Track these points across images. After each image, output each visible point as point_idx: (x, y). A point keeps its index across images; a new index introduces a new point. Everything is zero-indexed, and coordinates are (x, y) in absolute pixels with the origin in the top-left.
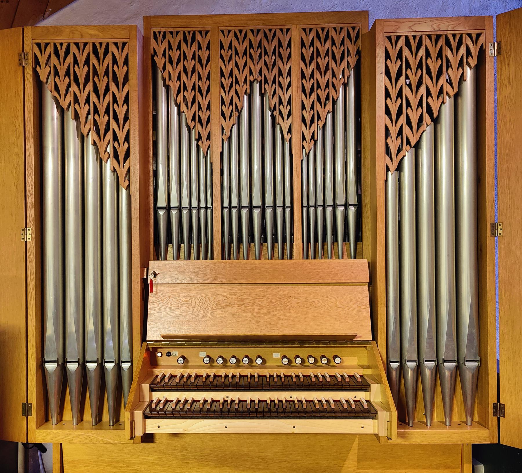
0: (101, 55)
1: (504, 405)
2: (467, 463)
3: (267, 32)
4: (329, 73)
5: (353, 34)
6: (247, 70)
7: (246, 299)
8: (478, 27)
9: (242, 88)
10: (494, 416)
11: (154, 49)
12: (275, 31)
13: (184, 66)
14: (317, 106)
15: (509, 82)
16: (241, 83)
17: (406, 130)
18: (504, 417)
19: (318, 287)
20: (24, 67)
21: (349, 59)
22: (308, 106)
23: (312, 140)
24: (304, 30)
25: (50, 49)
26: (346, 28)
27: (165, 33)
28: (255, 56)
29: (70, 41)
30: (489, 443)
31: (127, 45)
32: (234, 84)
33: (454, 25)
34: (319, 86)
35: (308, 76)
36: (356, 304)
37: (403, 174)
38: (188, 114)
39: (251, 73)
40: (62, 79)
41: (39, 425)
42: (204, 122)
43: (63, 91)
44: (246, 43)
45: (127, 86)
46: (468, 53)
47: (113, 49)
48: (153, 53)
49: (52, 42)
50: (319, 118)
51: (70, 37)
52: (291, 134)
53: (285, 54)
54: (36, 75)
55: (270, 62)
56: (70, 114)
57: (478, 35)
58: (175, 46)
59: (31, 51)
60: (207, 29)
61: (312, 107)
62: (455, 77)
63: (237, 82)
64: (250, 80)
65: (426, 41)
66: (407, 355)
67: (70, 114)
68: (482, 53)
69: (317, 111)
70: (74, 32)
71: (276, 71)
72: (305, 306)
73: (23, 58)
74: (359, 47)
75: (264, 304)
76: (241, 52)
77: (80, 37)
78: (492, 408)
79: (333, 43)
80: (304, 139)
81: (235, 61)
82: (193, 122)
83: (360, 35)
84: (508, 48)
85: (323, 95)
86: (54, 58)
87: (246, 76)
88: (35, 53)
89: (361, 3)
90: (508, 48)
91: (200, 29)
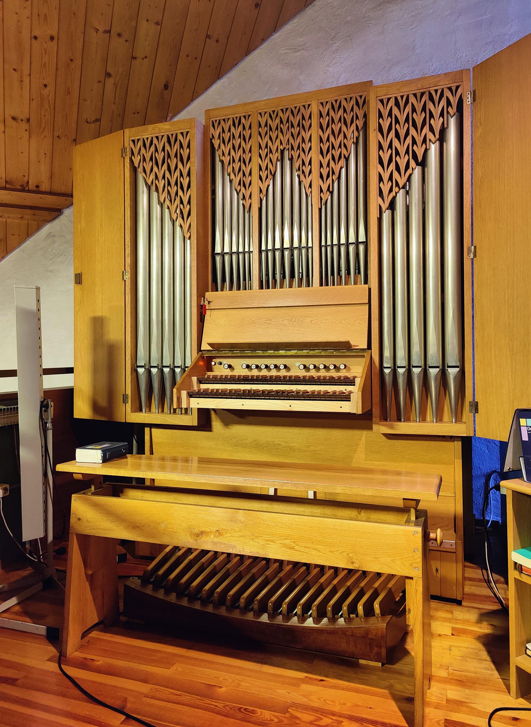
0: (173, 143)
1: (478, 402)
2: (457, 459)
3: (293, 109)
4: (342, 135)
5: (361, 102)
6: (278, 141)
7: (273, 319)
8: (456, 80)
9: (275, 156)
10: (470, 412)
11: (212, 134)
12: (299, 107)
13: (233, 144)
14: (332, 163)
15: (481, 124)
16: (274, 152)
17: (396, 175)
18: (478, 413)
19: (328, 308)
20: (124, 158)
21: (357, 122)
22: (325, 164)
23: (328, 192)
24: (322, 104)
25: (140, 143)
26: (355, 97)
27: (220, 120)
28: (285, 129)
29: (152, 135)
30: (466, 435)
31: (189, 133)
32: (269, 153)
33: (435, 82)
34: (333, 147)
35: (325, 140)
36: (357, 321)
37: (395, 212)
38: (236, 181)
39: (281, 143)
40: (148, 162)
41: (134, 411)
42: (247, 185)
43: (148, 172)
44: (278, 121)
45: (189, 163)
46: (449, 103)
47: (180, 137)
48: (211, 137)
49: (141, 138)
50: (333, 173)
51: (153, 133)
52: (311, 188)
53: (306, 124)
54: (131, 161)
55: (295, 133)
56: (153, 188)
57: (457, 87)
58: (226, 130)
59: (128, 146)
60: (249, 113)
61: (328, 165)
62: (437, 125)
63: (271, 151)
64: (281, 149)
65: (412, 99)
66: (399, 363)
67: (153, 188)
68: (460, 102)
69: (332, 167)
70: (155, 129)
71: (300, 139)
72: (317, 323)
73: (124, 151)
74: (365, 111)
75: (285, 322)
76: (274, 128)
77: (159, 132)
78: (469, 406)
79: (345, 111)
80: (321, 191)
81: (270, 135)
82: (239, 186)
83: (366, 102)
84: (480, 95)
85: (337, 154)
86: (143, 149)
87: (278, 146)
88: (131, 147)
89: (430, 69)
90: (480, 95)
91: (244, 114)
